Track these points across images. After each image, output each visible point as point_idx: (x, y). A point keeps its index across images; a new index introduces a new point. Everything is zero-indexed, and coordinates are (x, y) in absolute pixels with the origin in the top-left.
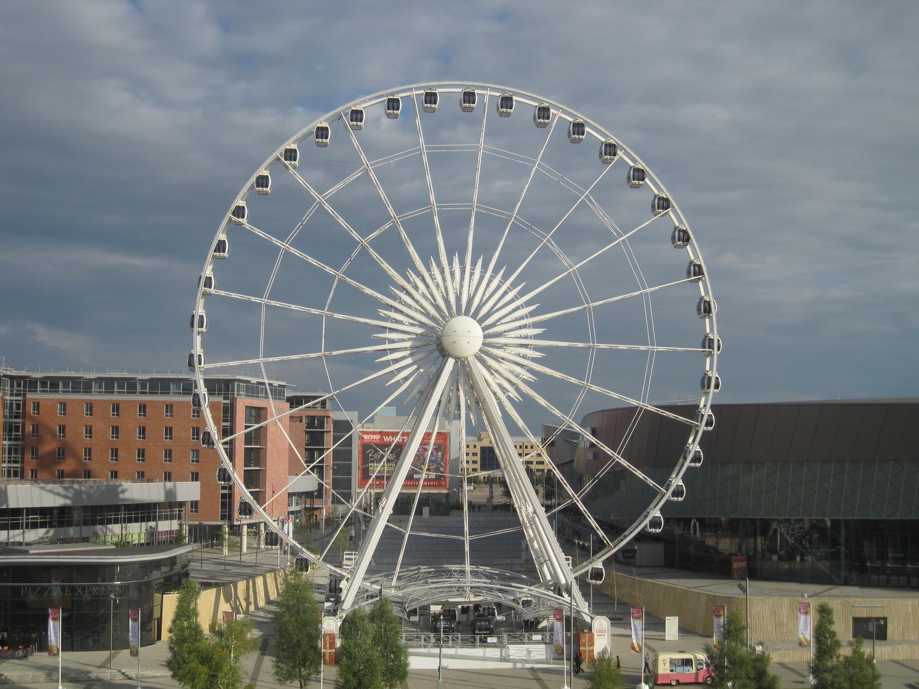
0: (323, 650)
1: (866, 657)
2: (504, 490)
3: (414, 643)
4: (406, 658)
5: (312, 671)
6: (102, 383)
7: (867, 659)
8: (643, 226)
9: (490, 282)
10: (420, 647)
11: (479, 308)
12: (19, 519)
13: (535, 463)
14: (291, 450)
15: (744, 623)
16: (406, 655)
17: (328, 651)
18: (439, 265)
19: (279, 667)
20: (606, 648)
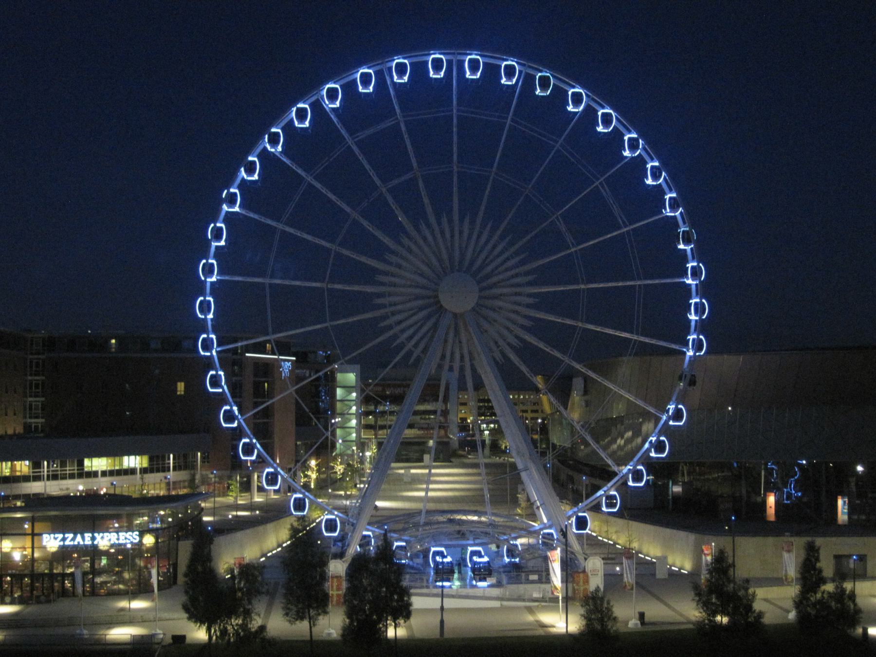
0: (331, 592)
1: (847, 592)
2: (402, 583)
3: (418, 584)
4: (409, 599)
5: (320, 611)
6: (548, 520)
7: (849, 595)
8: (541, 345)
9: (479, 237)
10: (422, 587)
11: (472, 263)
12: (40, 472)
13: (529, 412)
14: (297, 402)
15: (730, 561)
16: (409, 595)
17: (335, 593)
18: (429, 226)
19: (289, 609)
20: (598, 587)
